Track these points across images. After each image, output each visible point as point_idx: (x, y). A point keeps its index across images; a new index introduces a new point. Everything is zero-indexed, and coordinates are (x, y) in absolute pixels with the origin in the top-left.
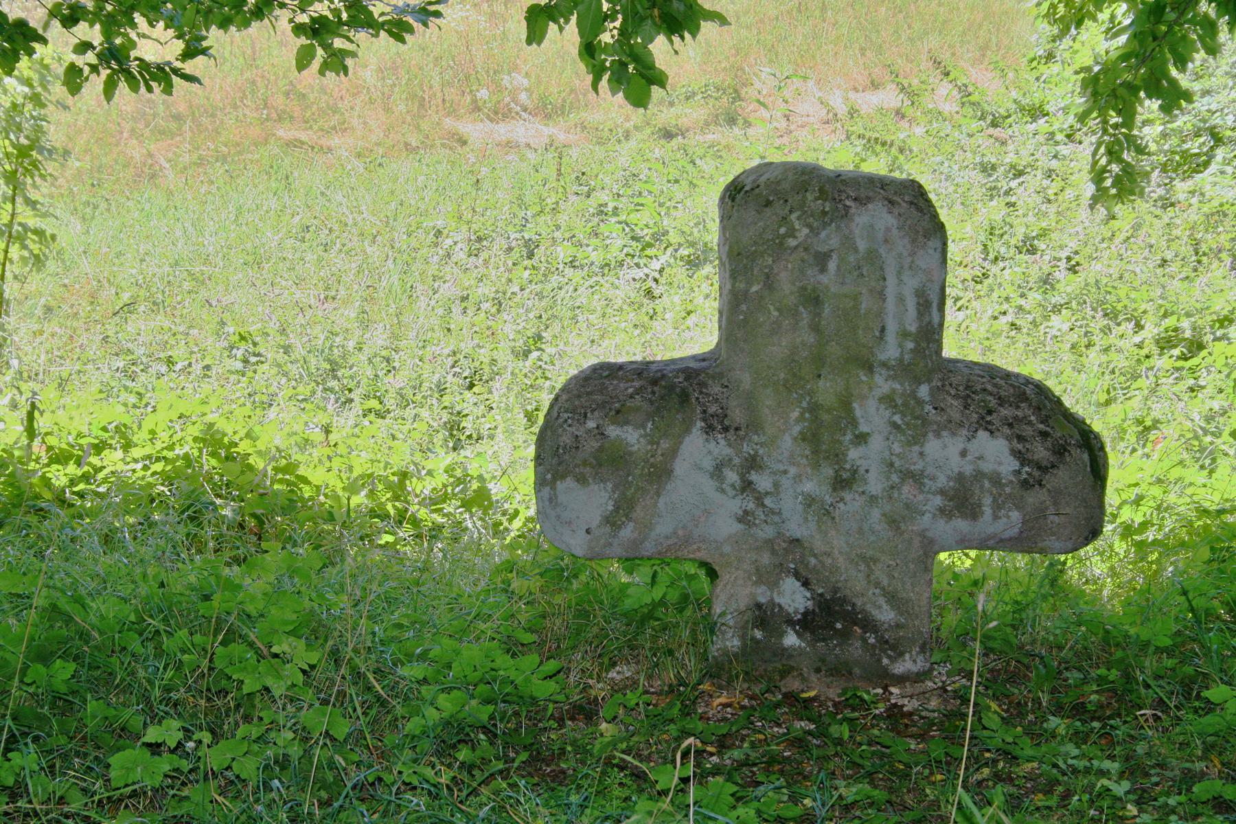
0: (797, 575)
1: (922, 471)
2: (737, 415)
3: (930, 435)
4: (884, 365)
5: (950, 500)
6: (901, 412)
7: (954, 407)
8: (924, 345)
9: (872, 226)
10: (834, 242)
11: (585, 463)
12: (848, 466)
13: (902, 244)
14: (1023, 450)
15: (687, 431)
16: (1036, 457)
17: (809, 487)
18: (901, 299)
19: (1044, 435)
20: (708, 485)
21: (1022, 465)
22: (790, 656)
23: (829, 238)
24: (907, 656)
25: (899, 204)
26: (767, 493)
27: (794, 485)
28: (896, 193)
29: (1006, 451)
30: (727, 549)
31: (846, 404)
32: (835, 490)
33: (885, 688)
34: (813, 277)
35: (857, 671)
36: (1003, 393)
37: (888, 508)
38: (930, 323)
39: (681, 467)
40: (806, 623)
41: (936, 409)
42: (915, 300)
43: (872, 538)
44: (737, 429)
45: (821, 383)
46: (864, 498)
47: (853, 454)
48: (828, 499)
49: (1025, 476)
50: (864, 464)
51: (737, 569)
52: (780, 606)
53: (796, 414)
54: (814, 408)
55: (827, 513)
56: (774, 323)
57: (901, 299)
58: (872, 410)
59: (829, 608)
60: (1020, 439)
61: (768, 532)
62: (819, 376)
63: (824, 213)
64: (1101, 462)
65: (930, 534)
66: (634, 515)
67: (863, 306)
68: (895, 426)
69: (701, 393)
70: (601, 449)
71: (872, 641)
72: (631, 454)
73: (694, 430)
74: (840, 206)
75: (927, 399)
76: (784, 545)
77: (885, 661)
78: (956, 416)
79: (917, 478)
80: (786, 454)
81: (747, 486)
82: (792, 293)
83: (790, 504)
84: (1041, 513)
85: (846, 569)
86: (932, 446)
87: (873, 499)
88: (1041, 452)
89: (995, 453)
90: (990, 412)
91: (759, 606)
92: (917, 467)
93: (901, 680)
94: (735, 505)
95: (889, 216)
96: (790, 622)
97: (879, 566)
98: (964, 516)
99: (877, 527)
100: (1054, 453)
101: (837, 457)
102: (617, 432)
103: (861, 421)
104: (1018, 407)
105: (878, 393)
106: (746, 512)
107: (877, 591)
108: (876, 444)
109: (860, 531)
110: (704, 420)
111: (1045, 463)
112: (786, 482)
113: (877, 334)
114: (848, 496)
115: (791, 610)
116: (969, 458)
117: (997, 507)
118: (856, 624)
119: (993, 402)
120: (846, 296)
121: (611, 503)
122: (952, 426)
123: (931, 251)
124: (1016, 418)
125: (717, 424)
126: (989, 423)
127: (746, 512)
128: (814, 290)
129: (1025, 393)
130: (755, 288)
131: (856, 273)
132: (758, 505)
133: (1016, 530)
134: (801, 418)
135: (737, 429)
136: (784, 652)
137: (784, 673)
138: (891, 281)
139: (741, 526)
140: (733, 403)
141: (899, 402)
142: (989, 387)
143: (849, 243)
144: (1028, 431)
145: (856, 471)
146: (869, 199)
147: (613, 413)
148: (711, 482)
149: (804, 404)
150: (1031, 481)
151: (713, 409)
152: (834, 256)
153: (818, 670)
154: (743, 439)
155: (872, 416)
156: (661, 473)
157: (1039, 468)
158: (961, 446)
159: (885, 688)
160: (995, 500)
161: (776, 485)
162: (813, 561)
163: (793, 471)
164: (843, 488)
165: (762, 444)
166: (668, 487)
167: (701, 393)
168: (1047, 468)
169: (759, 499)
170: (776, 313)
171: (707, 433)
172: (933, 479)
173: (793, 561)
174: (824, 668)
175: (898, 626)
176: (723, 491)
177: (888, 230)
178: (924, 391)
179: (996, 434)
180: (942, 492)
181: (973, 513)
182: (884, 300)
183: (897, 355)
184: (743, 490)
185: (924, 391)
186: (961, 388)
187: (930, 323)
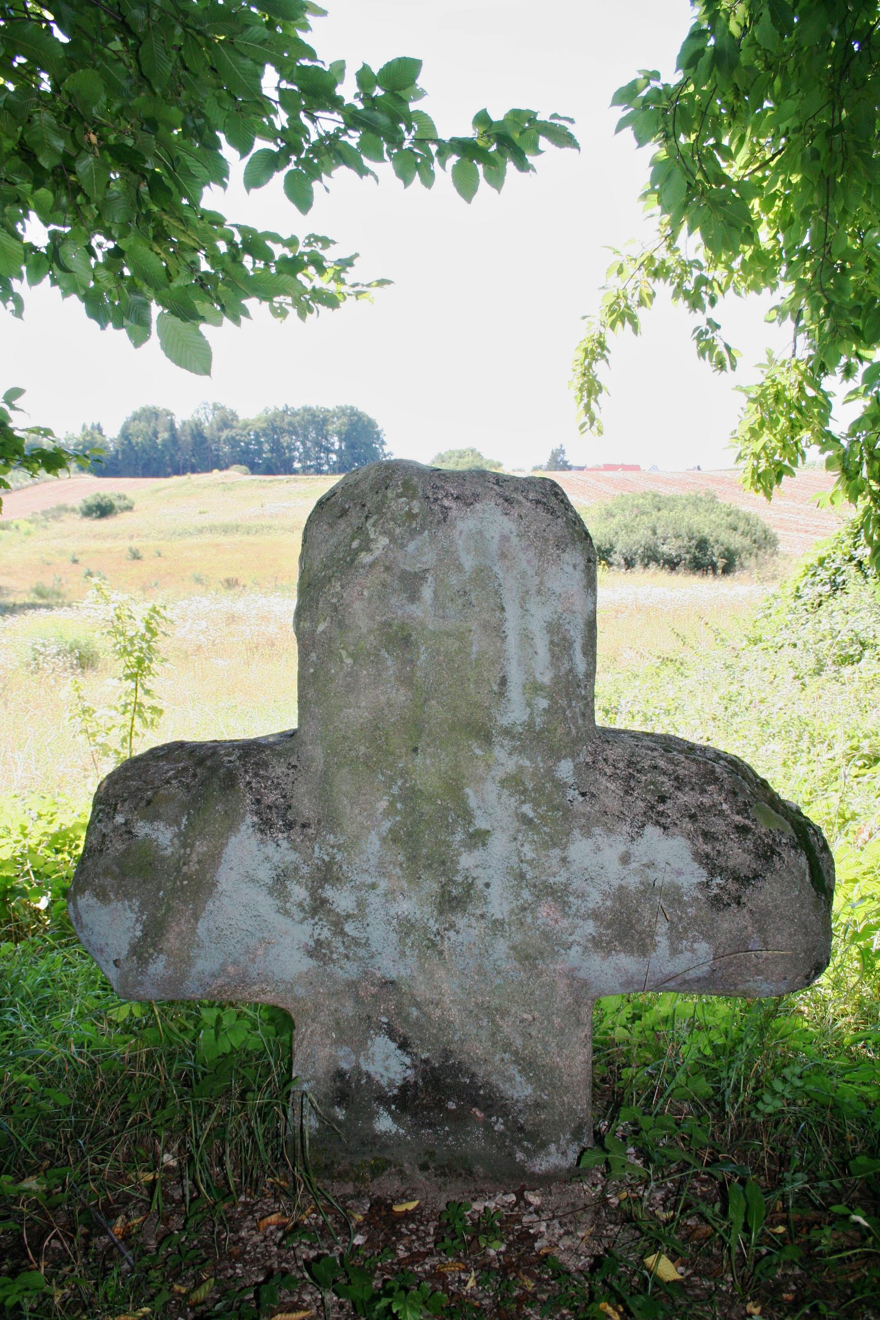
0: (391, 1033)
1: (566, 886)
2: (306, 807)
3: (576, 832)
4: (507, 732)
5: (607, 927)
6: (533, 800)
7: (610, 791)
8: (563, 702)
9: (480, 532)
10: (429, 558)
11: (106, 872)
12: (459, 879)
13: (525, 560)
14: (713, 854)
15: (232, 828)
16: (731, 864)
17: (405, 907)
18: (526, 637)
19: (742, 830)
20: (266, 904)
21: (712, 875)
22: (385, 1146)
23: (420, 553)
24: (553, 1147)
25: (519, 502)
26: (348, 916)
27: (385, 905)
28: (516, 489)
29: (687, 855)
30: (300, 991)
31: (454, 788)
32: (441, 913)
33: (520, 1196)
34: (401, 609)
35: (479, 1169)
36: (681, 772)
37: (518, 938)
38: (571, 670)
39: (227, 877)
40: (404, 1101)
41: (583, 794)
42: (547, 637)
43: (498, 981)
44: (304, 826)
45: (419, 760)
46: (483, 924)
47: (467, 861)
48: (433, 926)
49: (716, 891)
50: (482, 876)
51: (313, 1020)
52: (369, 1076)
53: (383, 804)
54: (410, 795)
55: (433, 945)
56: (349, 674)
57: (526, 637)
58: (492, 797)
59: (438, 1080)
60: (707, 836)
61: (350, 971)
62: (415, 750)
63: (411, 516)
64: (824, 867)
65: (581, 974)
66: (166, 945)
67: (474, 649)
68: (525, 820)
69: (256, 775)
70: (127, 852)
71: (499, 1127)
72: (163, 859)
73: (243, 828)
74: (436, 508)
75: (571, 781)
76: (374, 990)
77: (520, 1156)
78: (613, 804)
79: (558, 895)
80: (374, 861)
81: (319, 906)
82: (370, 631)
83: (379, 933)
84: (741, 945)
85: (463, 1025)
86: (580, 849)
87: (497, 925)
88: (738, 856)
89: (670, 857)
90: (662, 799)
91: (340, 1074)
92: (558, 879)
93: (544, 1181)
94: (303, 932)
95: (506, 518)
96: (383, 1099)
97: (510, 1020)
98: (629, 950)
99: (504, 966)
100: (758, 856)
101: (443, 864)
102: (147, 830)
103: (478, 813)
104: (703, 791)
105: (499, 773)
106: (318, 942)
107: (507, 1056)
108: (499, 845)
109: (481, 971)
110: (257, 813)
111: (744, 872)
112: (374, 900)
113: (495, 688)
114: (461, 922)
115: (384, 1082)
116: (634, 865)
117: (676, 936)
118: (476, 1105)
119: (667, 786)
120: (449, 635)
121: (139, 927)
122: (608, 820)
123: (569, 569)
124: (701, 806)
125: (277, 819)
126: (662, 814)
127: (318, 942)
128: (402, 628)
129: (713, 772)
130: (321, 628)
131: (460, 601)
132: (335, 934)
133: (706, 968)
134: (390, 812)
135: (304, 826)
136: (375, 1140)
137: (377, 1170)
138: (512, 612)
139: (312, 963)
140: (301, 789)
141: (530, 785)
142: (662, 763)
143: (448, 558)
144: (719, 826)
145: (471, 885)
146: (476, 497)
147: (143, 804)
148: (270, 900)
149: (395, 790)
150: (725, 897)
151: (271, 798)
152: (430, 579)
153: (424, 1167)
154: (312, 839)
155: (492, 805)
156: (198, 887)
157: (736, 879)
158: (622, 848)
159: (520, 1196)
160: (673, 927)
161: (361, 904)
162: (415, 1012)
163: (383, 884)
164: (453, 909)
165: (339, 847)
166: (210, 906)
167: (256, 775)
168: (747, 879)
169: (337, 925)
170: (349, 661)
171: (262, 831)
172: (583, 896)
173: (386, 1012)
174: (432, 1165)
175: (538, 1105)
176: (287, 913)
177: (505, 538)
178: (565, 769)
179: (673, 829)
180: (595, 915)
181: (642, 946)
182: (504, 639)
183: (525, 718)
184: (314, 911)
185: (565, 769)
186: (621, 765)
187: (571, 670)
